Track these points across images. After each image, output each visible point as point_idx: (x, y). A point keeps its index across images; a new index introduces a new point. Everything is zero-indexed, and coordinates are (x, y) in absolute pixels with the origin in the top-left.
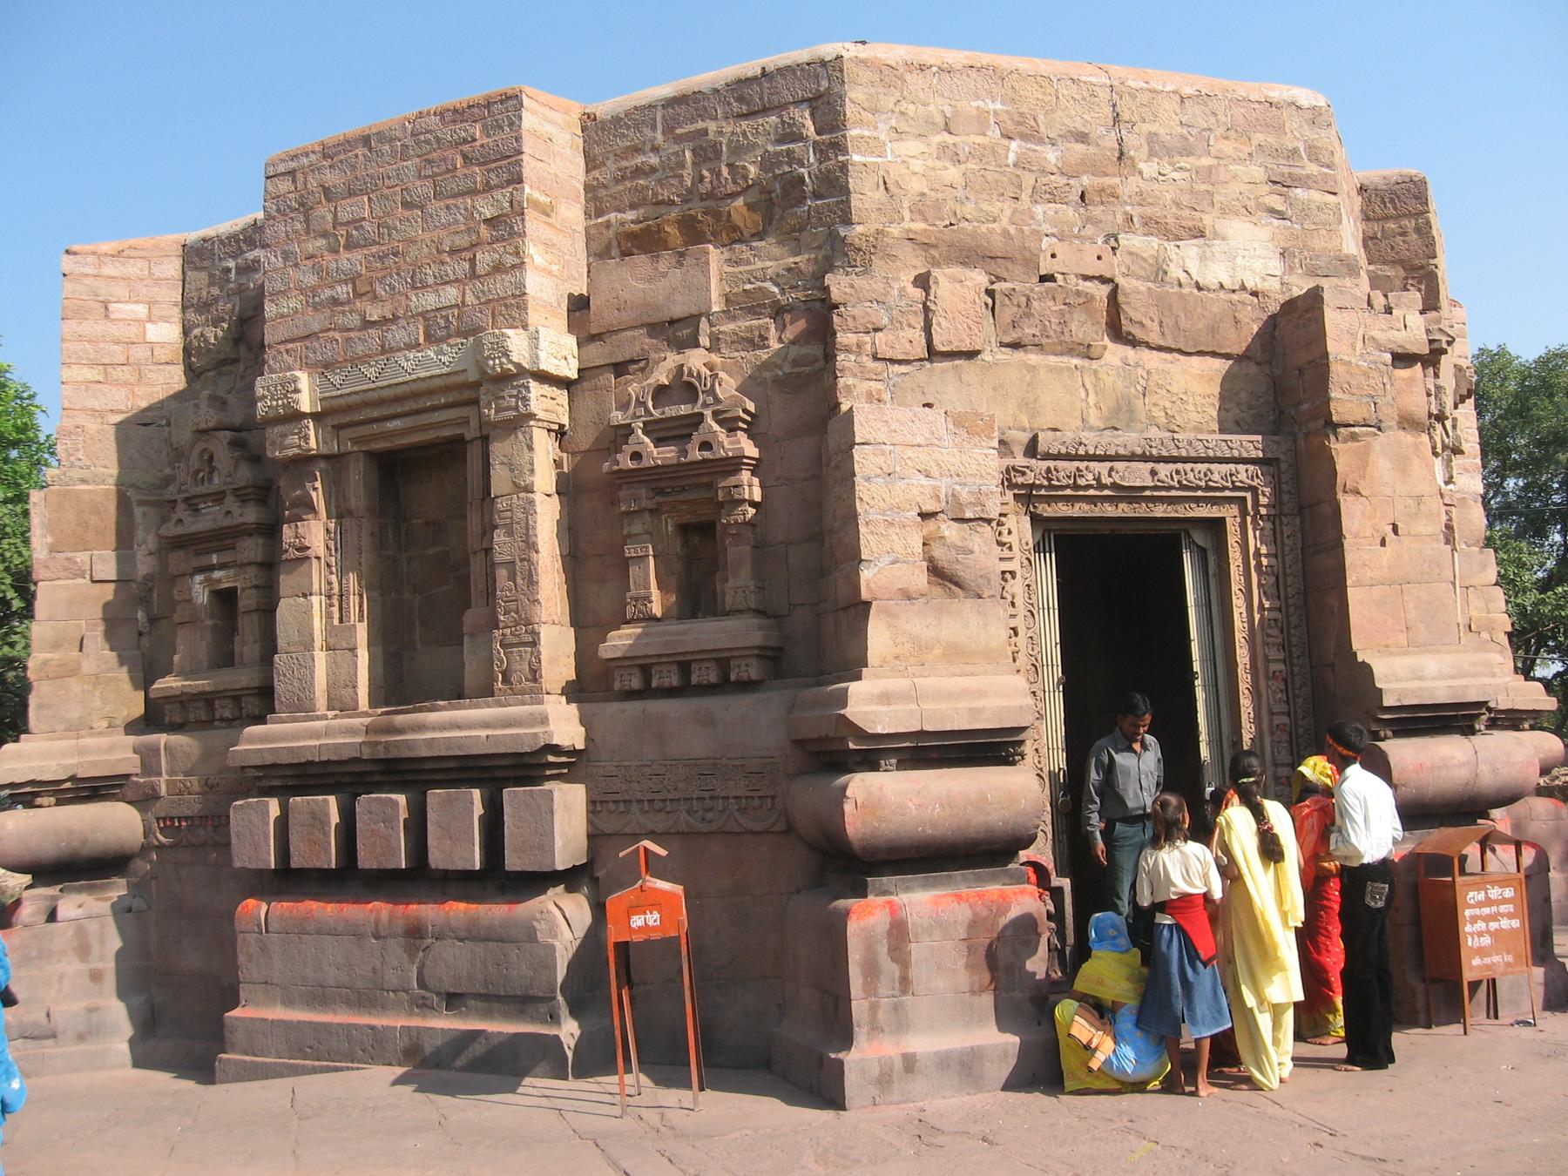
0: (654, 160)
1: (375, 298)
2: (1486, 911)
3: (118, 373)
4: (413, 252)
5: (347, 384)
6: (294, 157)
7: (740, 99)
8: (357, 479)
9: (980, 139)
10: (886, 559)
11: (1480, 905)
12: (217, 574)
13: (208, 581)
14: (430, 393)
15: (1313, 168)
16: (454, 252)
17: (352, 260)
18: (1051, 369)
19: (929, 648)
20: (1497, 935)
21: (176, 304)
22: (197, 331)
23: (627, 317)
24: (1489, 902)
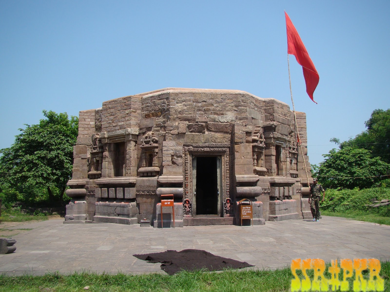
0: (149, 105)
1: (115, 123)
2: (246, 210)
3: (86, 129)
4: (119, 117)
5: (111, 134)
6: (106, 103)
7: (159, 97)
8: (112, 146)
9: (189, 103)
10: (166, 161)
11: (245, 209)
12: (97, 158)
13: (96, 159)
14: (120, 136)
15: (243, 103)
16: (123, 117)
17: (112, 117)
18: (196, 135)
19: (171, 172)
20: (247, 213)
21: (94, 119)
22: (97, 123)
23: (144, 126)
24: (246, 209)
